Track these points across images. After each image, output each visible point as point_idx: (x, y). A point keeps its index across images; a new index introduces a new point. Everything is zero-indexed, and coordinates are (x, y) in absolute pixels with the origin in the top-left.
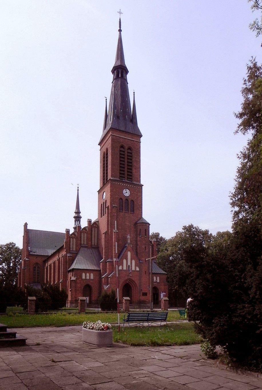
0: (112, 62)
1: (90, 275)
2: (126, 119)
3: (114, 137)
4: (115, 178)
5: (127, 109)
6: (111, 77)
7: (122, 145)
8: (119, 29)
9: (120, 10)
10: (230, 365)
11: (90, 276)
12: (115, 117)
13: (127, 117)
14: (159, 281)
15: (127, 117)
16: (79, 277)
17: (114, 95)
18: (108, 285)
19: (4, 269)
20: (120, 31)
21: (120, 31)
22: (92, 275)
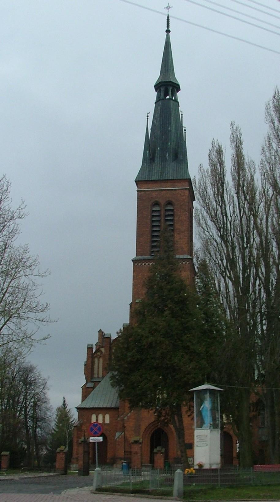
0: (155, 75)
1: (104, 417)
2: (166, 158)
3: (143, 193)
4: (142, 255)
5: (169, 144)
6: (154, 95)
7: (156, 201)
8: (166, 29)
9: (168, 4)
10: (36, 461)
11: (104, 419)
12: (146, 163)
13: (167, 155)
14: (91, 441)
15: (167, 155)
16: (85, 421)
17: (146, 133)
18: (150, 464)
19: (179, 195)
20: (168, 31)
21: (168, 31)
22: (107, 418)
